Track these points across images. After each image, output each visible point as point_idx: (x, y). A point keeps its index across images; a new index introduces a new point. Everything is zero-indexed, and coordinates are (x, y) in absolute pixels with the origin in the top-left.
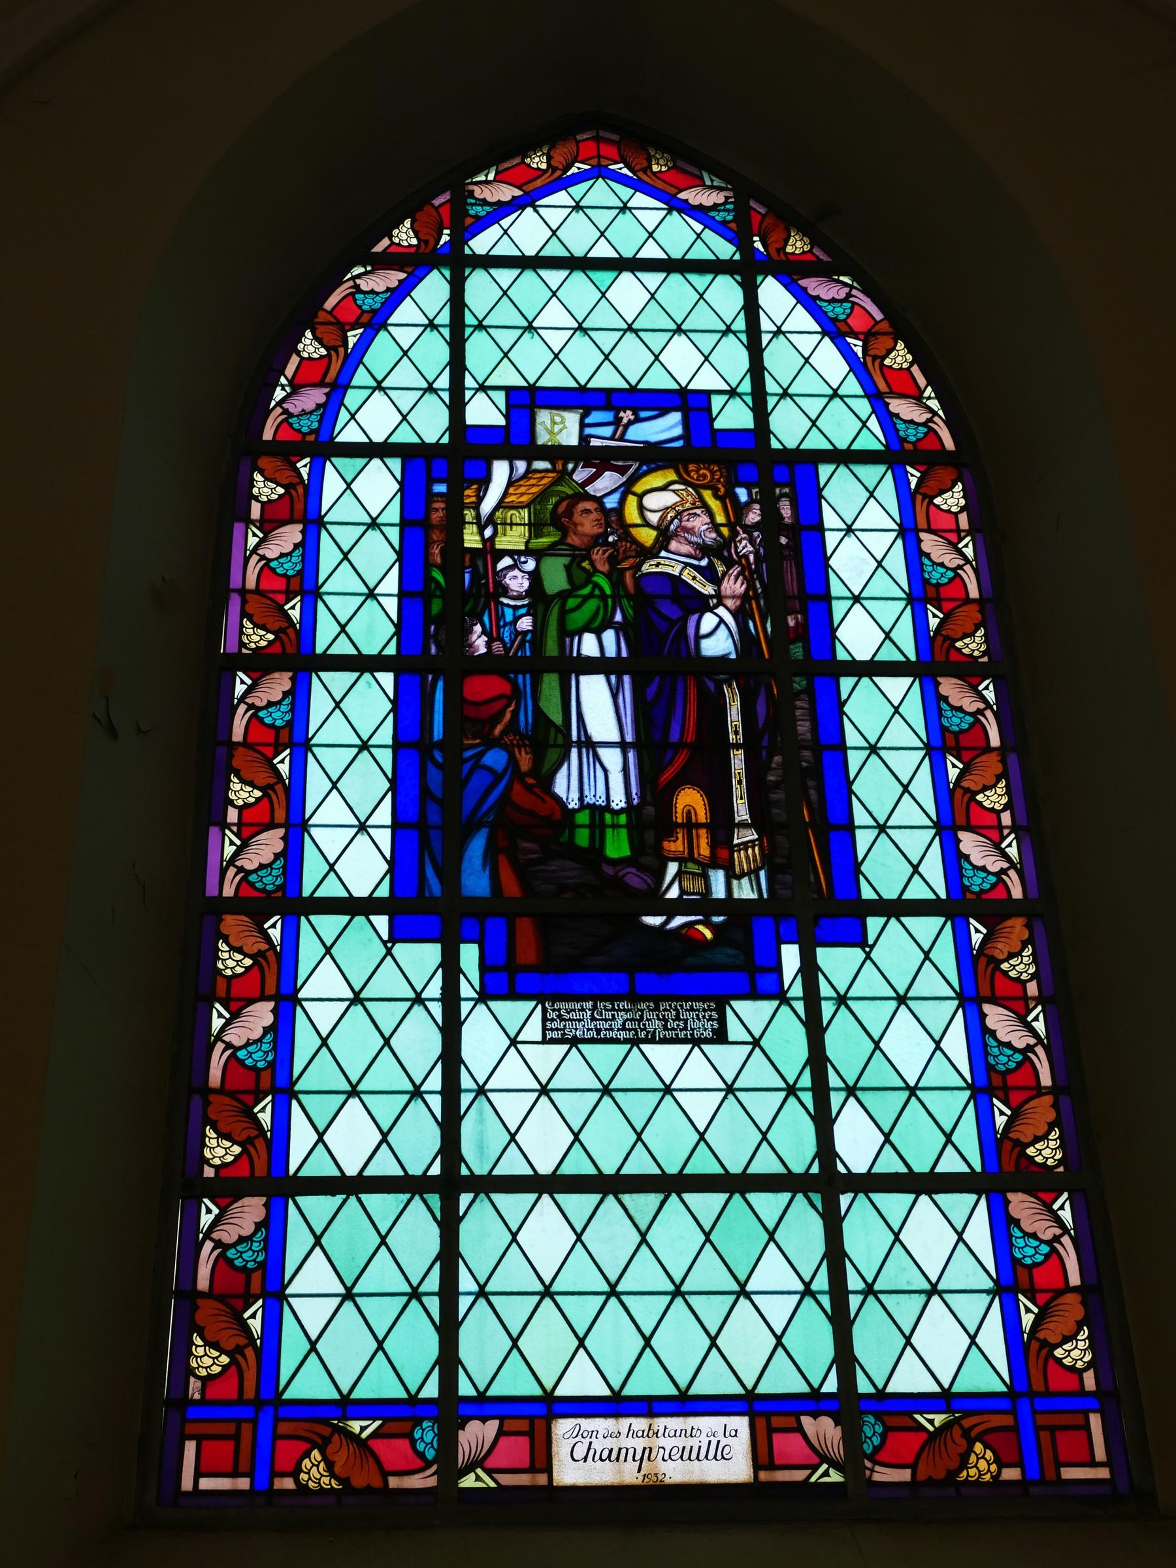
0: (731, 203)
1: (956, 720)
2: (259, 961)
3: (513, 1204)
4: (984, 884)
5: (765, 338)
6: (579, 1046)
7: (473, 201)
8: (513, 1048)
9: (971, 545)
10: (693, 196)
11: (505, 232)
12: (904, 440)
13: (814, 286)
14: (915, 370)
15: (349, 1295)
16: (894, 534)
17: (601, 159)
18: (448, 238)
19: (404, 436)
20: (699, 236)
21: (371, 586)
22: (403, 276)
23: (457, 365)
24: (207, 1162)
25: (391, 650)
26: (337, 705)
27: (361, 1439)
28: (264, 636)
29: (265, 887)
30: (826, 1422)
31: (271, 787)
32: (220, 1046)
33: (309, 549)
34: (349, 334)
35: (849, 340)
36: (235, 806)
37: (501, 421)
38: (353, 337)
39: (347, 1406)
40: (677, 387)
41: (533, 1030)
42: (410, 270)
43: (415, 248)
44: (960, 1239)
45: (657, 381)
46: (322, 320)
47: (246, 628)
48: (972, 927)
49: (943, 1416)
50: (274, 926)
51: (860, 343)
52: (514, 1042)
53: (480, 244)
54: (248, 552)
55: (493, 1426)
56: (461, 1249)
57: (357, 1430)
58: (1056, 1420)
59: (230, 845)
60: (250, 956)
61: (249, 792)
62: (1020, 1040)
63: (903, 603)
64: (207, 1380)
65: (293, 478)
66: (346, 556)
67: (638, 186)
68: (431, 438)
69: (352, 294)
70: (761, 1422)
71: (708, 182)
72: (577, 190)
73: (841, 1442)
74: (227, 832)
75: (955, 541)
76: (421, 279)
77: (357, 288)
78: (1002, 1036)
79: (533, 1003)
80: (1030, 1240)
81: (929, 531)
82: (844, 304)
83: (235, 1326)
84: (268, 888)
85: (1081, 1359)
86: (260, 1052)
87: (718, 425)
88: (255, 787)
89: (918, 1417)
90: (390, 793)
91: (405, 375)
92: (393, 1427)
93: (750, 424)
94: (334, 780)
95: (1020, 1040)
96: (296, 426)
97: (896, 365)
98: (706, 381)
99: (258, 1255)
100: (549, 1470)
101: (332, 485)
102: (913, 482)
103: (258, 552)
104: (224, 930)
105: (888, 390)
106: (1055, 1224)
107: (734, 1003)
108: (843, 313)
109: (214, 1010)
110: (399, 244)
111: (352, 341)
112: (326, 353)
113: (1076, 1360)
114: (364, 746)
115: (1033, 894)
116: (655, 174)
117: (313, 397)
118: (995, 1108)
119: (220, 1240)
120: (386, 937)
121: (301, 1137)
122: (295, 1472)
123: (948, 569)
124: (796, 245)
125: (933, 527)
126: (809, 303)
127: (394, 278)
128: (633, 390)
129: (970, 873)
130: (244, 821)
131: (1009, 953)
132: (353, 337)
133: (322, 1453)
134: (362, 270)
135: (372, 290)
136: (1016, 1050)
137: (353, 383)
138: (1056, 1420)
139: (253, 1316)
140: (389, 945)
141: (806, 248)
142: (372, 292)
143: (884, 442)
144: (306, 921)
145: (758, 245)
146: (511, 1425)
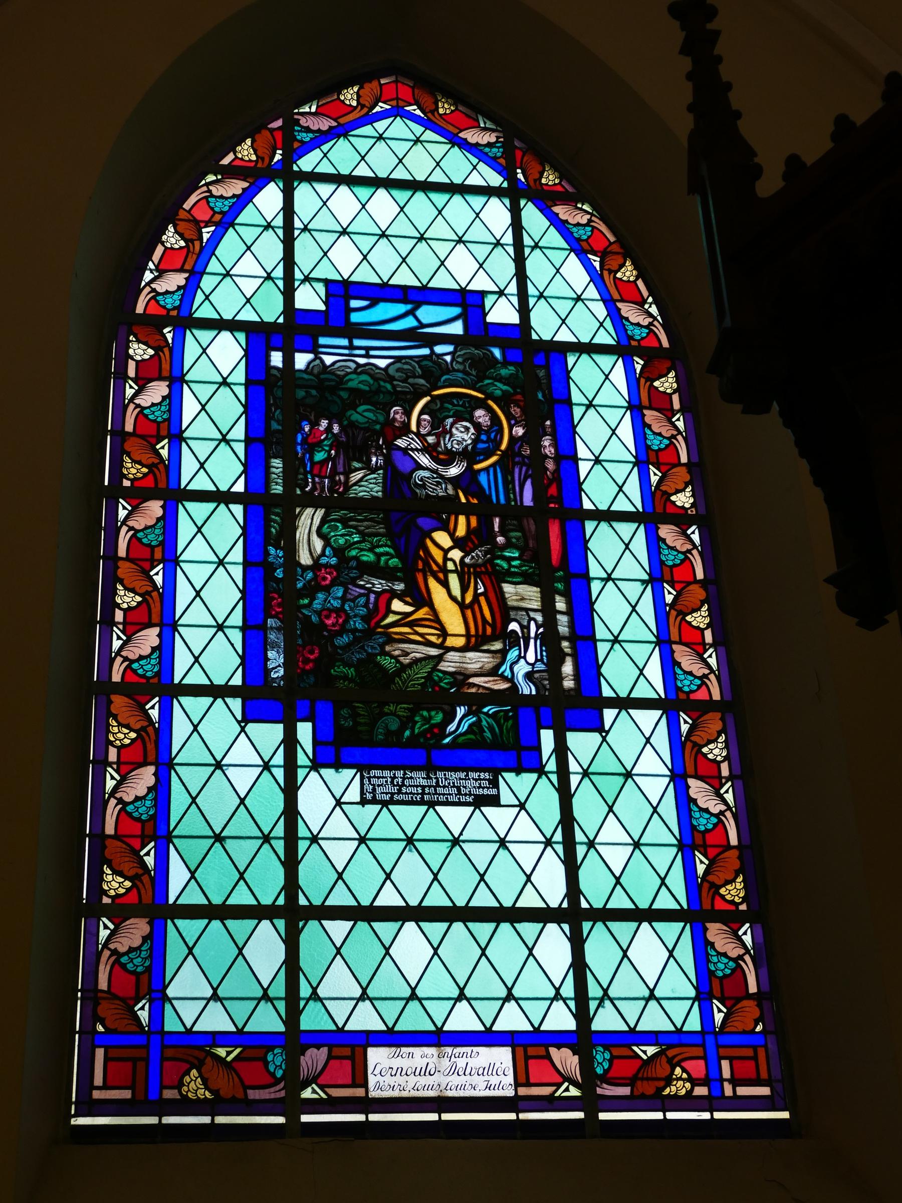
3: (338, 928)
5: (527, 251)
9: (714, 655)
10: (471, 136)
12: (631, 338)
13: (562, 211)
14: (640, 283)
17: (399, 101)
18: (280, 157)
19: (248, 315)
20: (475, 167)
22: (246, 185)
26: (199, 530)
27: (227, 1061)
28: (140, 469)
31: (148, 593)
33: (174, 401)
34: (204, 230)
37: (322, 307)
38: (207, 233)
40: (458, 288)
41: (354, 794)
43: (254, 163)
45: (442, 281)
47: (126, 462)
48: (665, 590)
49: (653, 1048)
51: (598, 259)
52: (339, 803)
53: (306, 163)
56: (295, 260)
59: (117, 640)
60: (134, 731)
62: (715, 807)
63: (668, 779)
66: (202, 465)
67: (428, 124)
68: (269, 318)
70: (520, 1050)
71: (482, 125)
72: (381, 125)
74: (115, 628)
75: (701, 652)
79: (355, 771)
80: (722, 958)
81: (680, 643)
82: (586, 228)
85: (720, 755)
86: (139, 958)
87: (490, 319)
88: (136, 593)
89: (635, 1048)
90: (244, 358)
92: (251, 1053)
94: (197, 655)
95: (699, 670)
96: (162, 303)
98: (481, 283)
99: (145, 961)
100: (365, 1085)
101: (191, 350)
105: (619, 298)
107: (504, 774)
110: (242, 159)
111: (206, 237)
113: (717, 756)
115: (728, 698)
116: (441, 115)
117: (176, 280)
120: (240, 718)
121: (188, 465)
122: (179, 1085)
123: (679, 552)
124: (550, 178)
125: (699, 773)
129: (682, 677)
130: (122, 760)
131: (708, 740)
134: (214, 178)
137: (208, 270)
140: (243, 724)
142: (221, 197)
144: (172, 924)
145: (520, 176)
146: (337, 1051)
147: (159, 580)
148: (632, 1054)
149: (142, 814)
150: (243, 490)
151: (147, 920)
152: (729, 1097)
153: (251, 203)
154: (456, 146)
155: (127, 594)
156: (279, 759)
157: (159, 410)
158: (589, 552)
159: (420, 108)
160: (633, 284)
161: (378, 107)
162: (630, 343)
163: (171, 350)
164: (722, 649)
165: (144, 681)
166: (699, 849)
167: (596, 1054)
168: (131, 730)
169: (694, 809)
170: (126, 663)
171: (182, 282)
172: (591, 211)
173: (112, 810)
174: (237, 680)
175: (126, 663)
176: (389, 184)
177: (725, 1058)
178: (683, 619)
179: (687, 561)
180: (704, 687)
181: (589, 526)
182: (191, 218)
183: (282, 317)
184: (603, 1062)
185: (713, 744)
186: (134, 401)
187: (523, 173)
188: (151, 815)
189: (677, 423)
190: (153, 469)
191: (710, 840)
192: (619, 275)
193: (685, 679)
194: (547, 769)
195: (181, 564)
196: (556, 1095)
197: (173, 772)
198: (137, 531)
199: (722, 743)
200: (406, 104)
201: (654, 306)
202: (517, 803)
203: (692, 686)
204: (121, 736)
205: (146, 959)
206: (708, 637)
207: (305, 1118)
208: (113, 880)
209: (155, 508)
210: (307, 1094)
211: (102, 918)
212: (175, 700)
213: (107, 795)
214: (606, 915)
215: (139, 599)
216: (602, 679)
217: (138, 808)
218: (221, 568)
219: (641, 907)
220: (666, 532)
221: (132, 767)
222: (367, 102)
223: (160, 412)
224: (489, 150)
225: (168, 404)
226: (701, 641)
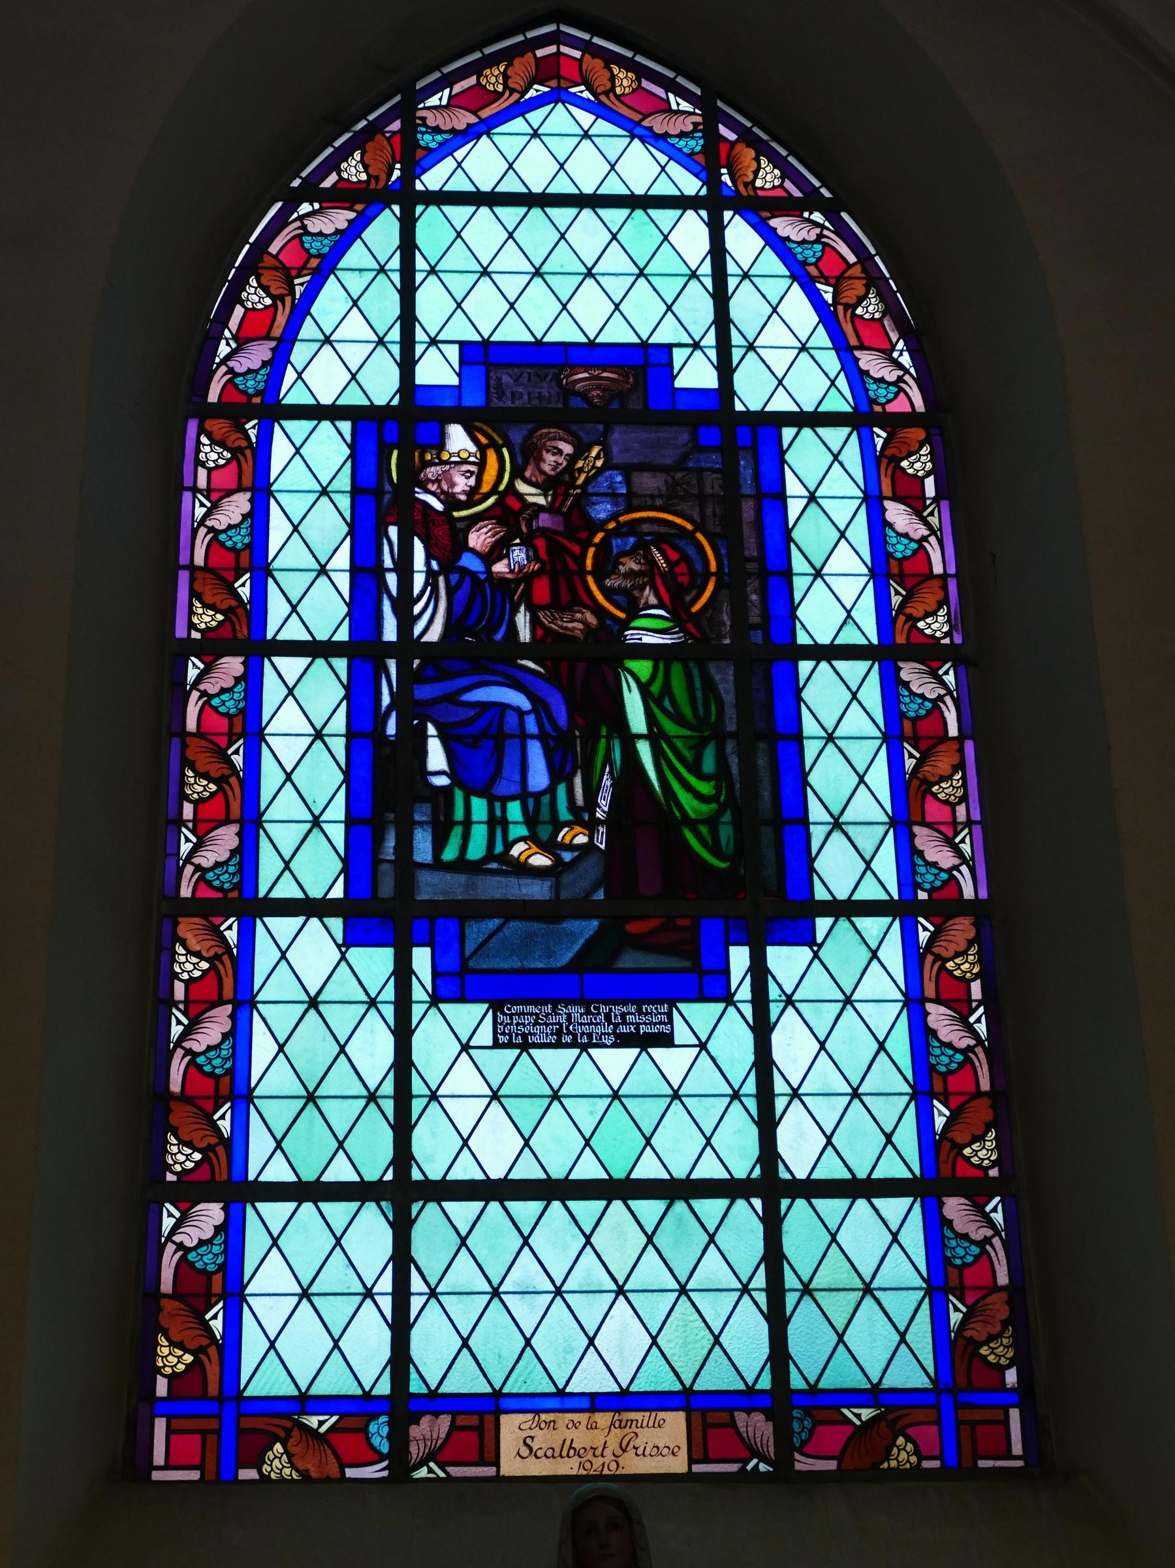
2: (230, 617)
3: (462, 1211)
6: (531, 1051)
7: (423, 129)
11: (459, 165)
12: (874, 401)
13: (783, 226)
16: (900, 1005)
19: (354, 398)
20: (663, 168)
21: (328, 334)
23: (408, 318)
24: (169, 1168)
25: (338, 892)
30: (758, 1417)
33: (258, 519)
36: (190, 801)
37: (454, 381)
39: (306, 1402)
41: (485, 1036)
42: (359, 207)
43: (365, 184)
50: (230, 928)
52: (466, 1048)
53: (433, 179)
54: (196, 524)
57: (315, 1425)
58: (977, 1415)
60: (199, 1151)
61: (211, 616)
67: (600, 110)
68: (380, 400)
69: (299, 236)
70: (697, 1417)
72: (535, 117)
75: (950, 834)
76: (371, 220)
78: (959, 1227)
82: (815, 246)
84: (217, 1071)
86: (210, 1254)
87: (679, 383)
89: (846, 1411)
92: (351, 1422)
93: (714, 384)
95: (931, 691)
97: (868, 314)
102: (879, 443)
104: (173, 1120)
106: (986, 1225)
107: (679, 1005)
108: (813, 256)
116: (618, 97)
117: (259, 354)
119: (199, 864)
120: (340, 941)
124: (768, 177)
125: (942, 997)
127: (341, 218)
128: (591, 345)
130: (191, 998)
132: (300, 284)
133: (284, 1446)
135: (321, 232)
136: (957, 1050)
138: (977, 1415)
139: (222, 1117)
140: (343, 949)
142: (320, 234)
145: (726, 179)
148: (841, 1418)
149: (224, 883)
150: (341, 896)
153: (359, 240)
155: (198, 782)
157: (239, 534)
158: (808, 789)
160: (878, 324)
162: (872, 409)
165: (220, 895)
168: (195, 1149)
169: (933, 1044)
170: (180, 1253)
171: (268, 356)
173: (169, 1260)
174: (343, 635)
182: (278, 265)
183: (391, 1171)
185: (932, 618)
187: (731, 174)
188: (234, 884)
189: (929, 519)
191: (970, 1278)
192: (859, 311)
193: (898, 543)
194: (736, 998)
195: (259, 1006)
198: (219, 532)
199: (1008, 1337)
200: (569, 84)
201: (906, 354)
202: (697, 1042)
205: (234, 874)
206: (976, 989)
209: (233, 665)
212: (276, 424)
213: (172, 1045)
214: (812, 1189)
216: (803, 706)
217: (202, 1256)
218: (318, 743)
220: (954, 1207)
221: (205, 1006)
222: (516, 82)
226: (965, 997)
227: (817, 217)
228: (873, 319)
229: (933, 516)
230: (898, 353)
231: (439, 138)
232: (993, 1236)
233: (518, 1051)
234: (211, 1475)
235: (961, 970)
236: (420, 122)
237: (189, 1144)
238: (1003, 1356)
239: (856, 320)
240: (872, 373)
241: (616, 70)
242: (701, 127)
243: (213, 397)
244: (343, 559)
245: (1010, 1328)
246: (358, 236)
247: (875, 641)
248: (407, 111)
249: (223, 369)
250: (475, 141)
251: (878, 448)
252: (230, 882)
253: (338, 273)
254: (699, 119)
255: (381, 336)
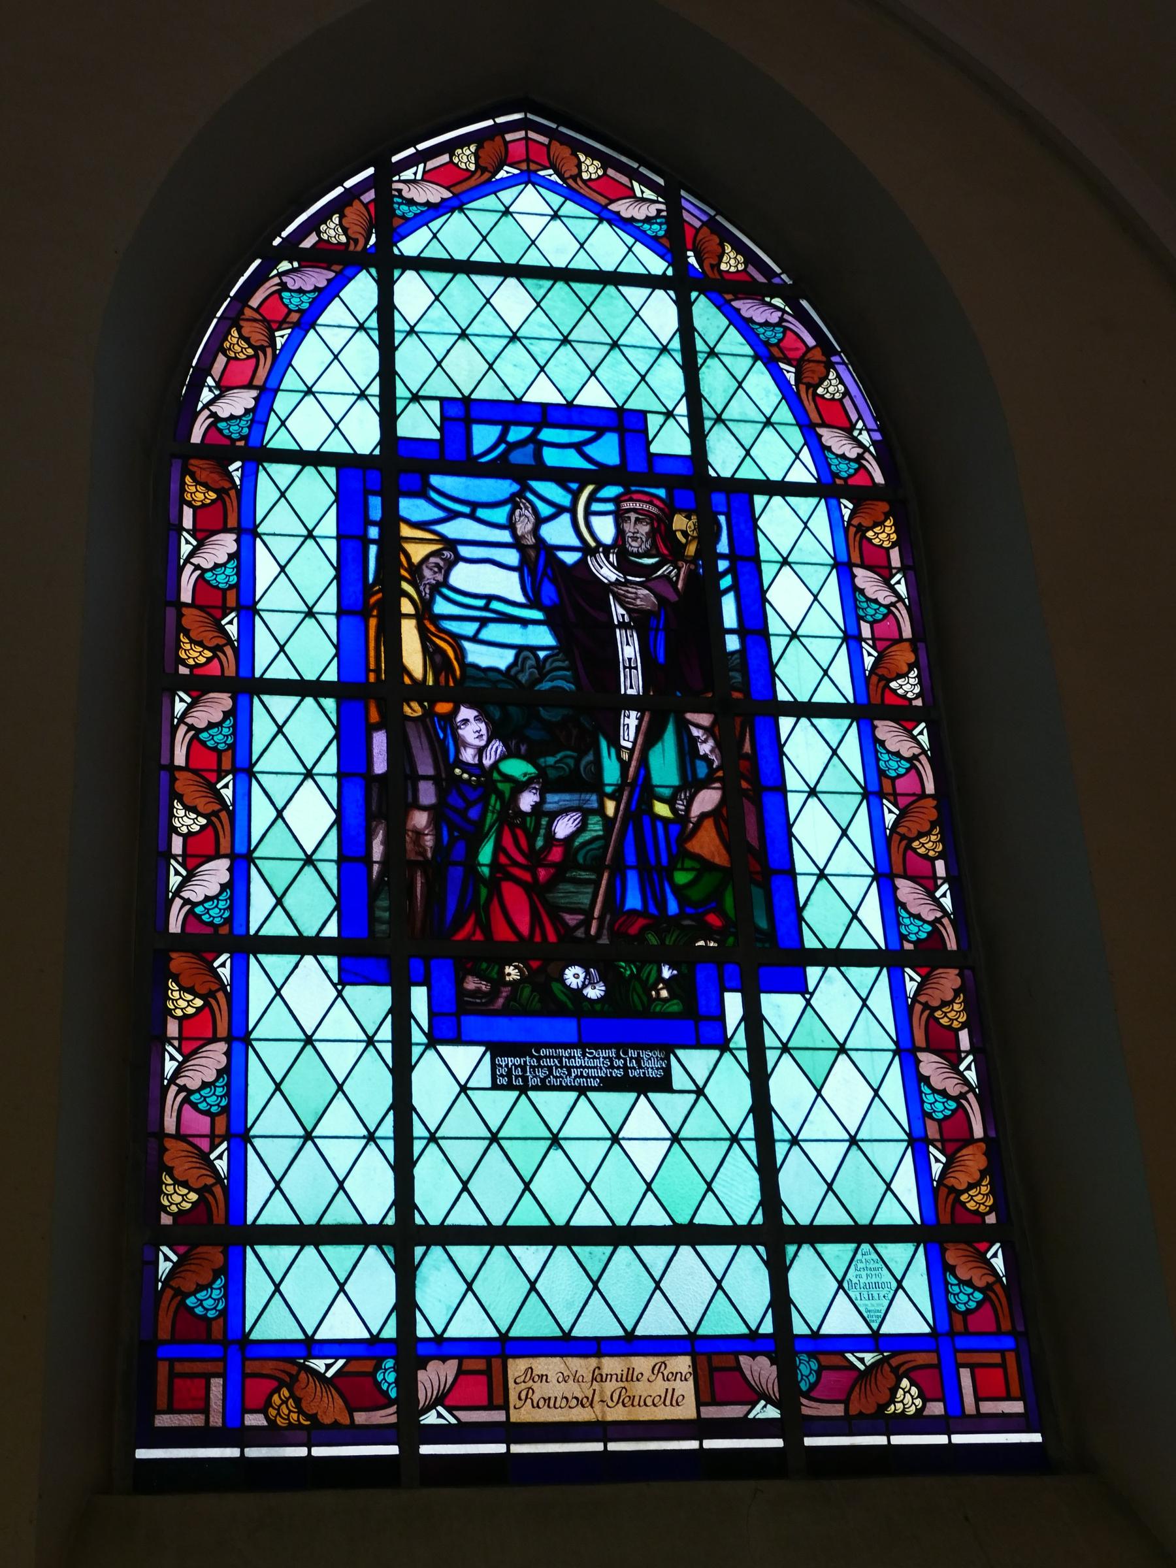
0: (663, 217)
1: (914, 929)
4: (877, 615)
7: (400, 200)
8: (463, 1094)
9: (903, 581)
11: (435, 236)
12: (835, 475)
13: (748, 308)
15: (308, 1136)
16: (905, 1144)
19: (336, 445)
20: (630, 249)
23: (387, 373)
24: (164, 1209)
26: (282, 648)
29: (206, 1314)
30: (763, 1361)
31: (215, 814)
32: (178, 902)
33: (244, 561)
35: (782, 365)
36: (179, 834)
37: (436, 435)
39: (311, 1346)
41: (483, 1077)
42: (338, 268)
44: (865, 1005)
46: (247, 317)
48: (885, 808)
50: (223, 965)
51: (793, 370)
52: (464, 1089)
53: (410, 246)
55: (452, 1365)
60: (195, 1191)
61: (193, 819)
64: (188, 837)
65: (219, 639)
67: (571, 194)
70: (702, 1359)
72: (507, 195)
73: (776, 1381)
74: (172, 862)
76: (350, 280)
77: (284, 287)
78: (870, 593)
80: (965, 1287)
82: (777, 329)
83: (209, 795)
87: (655, 448)
88: (199, 814)
89: (849, 1356)
91: (335, 379)
95: (908, 749)
100: (505, 1407)
103: (182, 894)
105: (820, 422)
107: (680, 1053)
109: (182, 538)
111: (280, 342)
112: (253, 353)
114: (309, 860)
116: (584, 181)
118: (931, 1155)
119: (199, 564)
120: (336, 980)
126: (745, 326)
130: (185, 1035)
131: (919, 832)
137: (281, 388)
140: (340, 987)
141: (741, 267)
143: (816, 476)
145: (692, 260)
147: (225, 973)
148: (847, 1364)
150: (335, 679)
151: (230, 695)
152: (970, 1416)
153: (337, 299)
154: (605, 222)
156: (387, 1129)
159: (557, 173)
161: (502, 171)
163: (239, 493)
164: (911, 573)
166: (889, 797)
167: (800, 1363)
168: (191, 1189)
170: (187, 907)
171: (251, 404)
172: (783, 307)
175: (187, 907)
176: (519, 272)
177: (965, 1366)
178: (887, 686)
179: (891, 616)
180: (913, 771)
181: (785, 723)
184: (809, 1375)
186: (186, 720)
188: (225, 919)
190: (209, 999)
191: (901, 786)
196: (749, 1417)
197: (253, 870)
198: (204, 571)
200: (540, 167)
203: (920, 933)
204: (183, 1004)
207: (425, 1449)
208: (181, 998)
210: (431, 1418)
211: (161, 1248)
215: (203, 821)
216: (777, 681)
219: (799, 699)
223: (214, 1098)
224: (648, 227)
225: (229, 898)
226: (886, 564)
227: (777, 302)
228: (833, 399)
229: (971, 1070)
230: (858, 432)
231: (414, 208)
232: (967, 1092)
233: (516, 1093)
234: (219, 1367)
235: (948, 1018)
236: (397, 194)
237: (191, 991)
238: (983, 1204)
239: (817, 399)
240: (834, 449)
241: (582, 157)
242: (720, 774)
243: (196, 437)
244: (329, 526)
245: (962, 995)
246: (337, 295)
247: (852, 700)
248: (382, 182)
249: (206, 413)
250: (449, 214)
251: (846, 518)
252: (221, 916)
253: (318, 328)
254: (663, 207)
255: (363, 388)
